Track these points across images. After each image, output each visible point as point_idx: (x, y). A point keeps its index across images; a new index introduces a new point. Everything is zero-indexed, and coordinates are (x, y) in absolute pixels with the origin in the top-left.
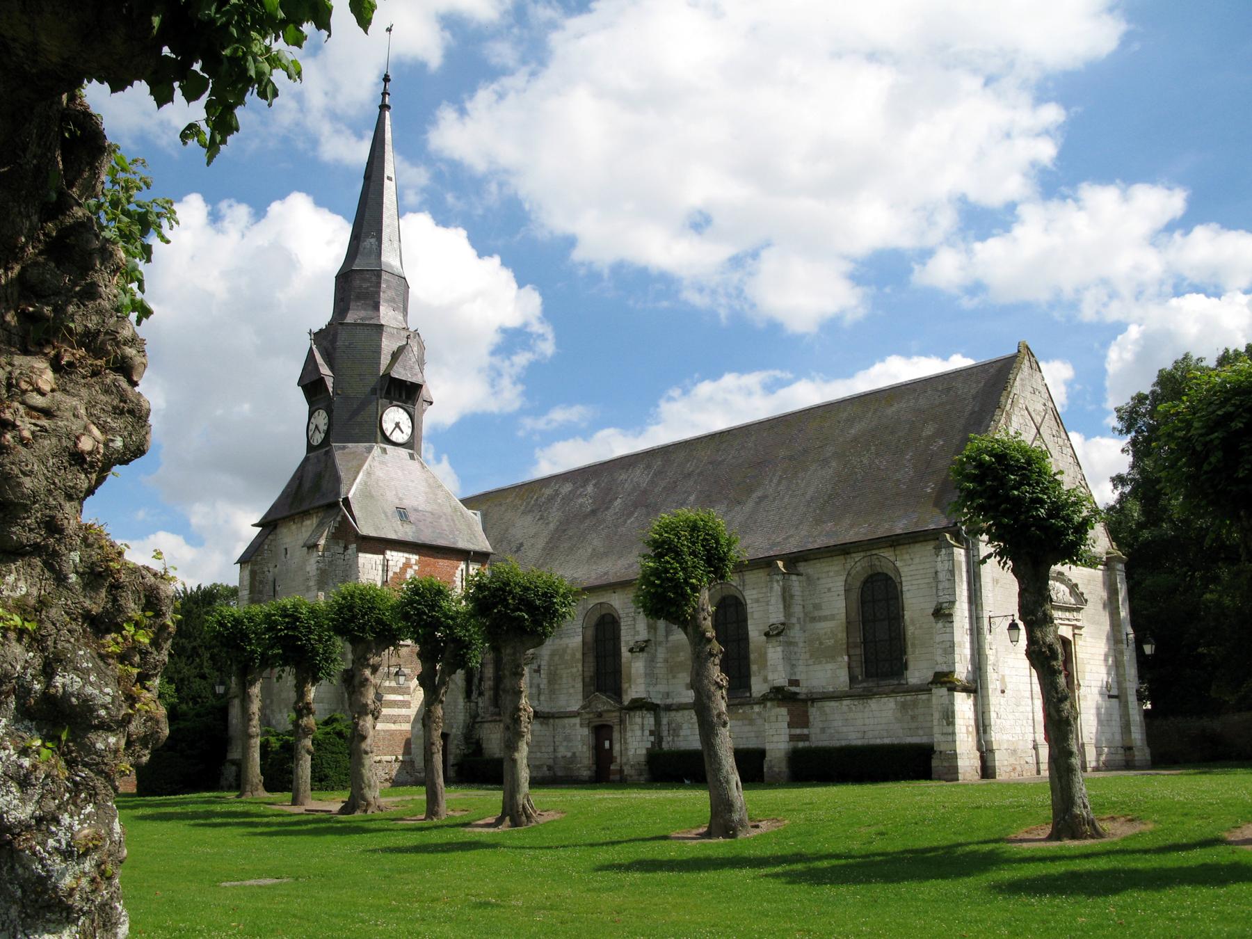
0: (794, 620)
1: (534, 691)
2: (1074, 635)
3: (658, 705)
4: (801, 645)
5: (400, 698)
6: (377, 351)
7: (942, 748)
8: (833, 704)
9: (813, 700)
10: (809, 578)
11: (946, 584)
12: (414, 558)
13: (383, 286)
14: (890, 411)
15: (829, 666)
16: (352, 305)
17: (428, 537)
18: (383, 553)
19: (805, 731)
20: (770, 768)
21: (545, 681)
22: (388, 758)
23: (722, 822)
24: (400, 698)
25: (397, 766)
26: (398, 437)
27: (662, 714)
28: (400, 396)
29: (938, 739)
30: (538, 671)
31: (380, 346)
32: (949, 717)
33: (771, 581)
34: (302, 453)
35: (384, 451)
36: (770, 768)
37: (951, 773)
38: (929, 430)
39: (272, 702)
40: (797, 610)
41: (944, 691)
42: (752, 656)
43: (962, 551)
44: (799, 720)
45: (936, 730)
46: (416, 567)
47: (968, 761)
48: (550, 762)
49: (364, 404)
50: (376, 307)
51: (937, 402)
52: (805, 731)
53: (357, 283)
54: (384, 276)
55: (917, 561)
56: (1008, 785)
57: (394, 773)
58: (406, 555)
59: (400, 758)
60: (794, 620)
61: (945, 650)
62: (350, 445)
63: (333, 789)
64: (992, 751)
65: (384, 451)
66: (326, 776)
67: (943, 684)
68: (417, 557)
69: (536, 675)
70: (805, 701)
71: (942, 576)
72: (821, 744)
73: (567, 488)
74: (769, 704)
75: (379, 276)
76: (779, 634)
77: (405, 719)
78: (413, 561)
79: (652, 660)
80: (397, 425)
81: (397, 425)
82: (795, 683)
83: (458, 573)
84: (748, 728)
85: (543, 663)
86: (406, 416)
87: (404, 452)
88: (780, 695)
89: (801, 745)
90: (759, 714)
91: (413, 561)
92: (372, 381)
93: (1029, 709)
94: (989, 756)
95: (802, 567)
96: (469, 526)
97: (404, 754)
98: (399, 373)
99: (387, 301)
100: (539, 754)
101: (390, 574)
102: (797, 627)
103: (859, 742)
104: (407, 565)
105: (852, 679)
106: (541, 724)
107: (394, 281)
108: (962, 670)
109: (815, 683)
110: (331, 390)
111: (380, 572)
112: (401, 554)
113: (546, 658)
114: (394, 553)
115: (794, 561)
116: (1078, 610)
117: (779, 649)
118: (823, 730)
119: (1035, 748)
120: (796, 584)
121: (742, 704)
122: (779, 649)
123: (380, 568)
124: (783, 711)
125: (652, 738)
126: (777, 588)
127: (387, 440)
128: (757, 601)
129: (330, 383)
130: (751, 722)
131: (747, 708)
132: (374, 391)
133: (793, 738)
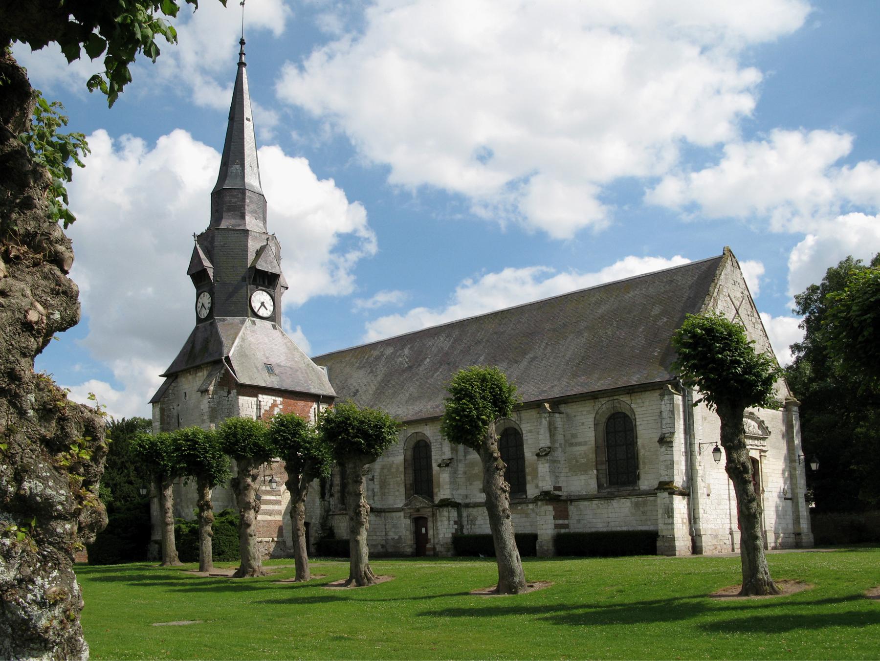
0: (557, 445)
1: (370, 493)
2: (761, 456)
3: (459, 504)
4: (562, 462)
5: (274, 498)
6: (245, 250)
8: (586, 503)
9: (572, 501)
10: (568, 415)
11: (668, 421)
12: (279, 400)
13: (247, 201)
14: (628, 296)
15: (583, 477)
16: (225, 215)
17: (288, 385)
18: (256, 396)
19: (566, 522)
20: (541, 547)
21: (378, 487)
22: (267, 539)
24: (274, 498)
25: (273, 545)
26: (263, 312)
27: (463, 510)
28: (264, 282)
29: (661, 528)
30: (372, 479)
31: (247, 246)
32: (669, 512)
33: (541, 417)
34: (194, 324)
35: (254, 323)
36: (541, 547)
37: (671, 550)
38: (656, 311)
39: (181, 500)
40: (560, 438)
41: (666, 494)
42: (527, 470)
43: (680, 397)
45: (660, 521)
46: (281, 407)
48: (383, 542)
49: (237, 289)
50: (243, 217)
52: (566, 522)
53: (227, 199)
54: (248, 194)
55: (647, 403)
56: (711, 559)
57: (271, 550)
58: (273, 398)
59: (276, 539)
60: (557, 445)
61: (667, 466)
62: (228, 318)
63: (228, 560)
64: (700, 536)
65: (254, 323)
66: (223, 552)
67: (665, 490)
68: (281, 399)
69: (370, 482)
70: (566, 501)
72: (577, 530)
73: (390, 350)
74: (540, 503)
75: (244, 194)
76: (546, 455)
77: (278, 512)
78: (279, 402)
79: (455, 472)
80: (263, 304)
81: (263, 304)
83: (312, 411)
85: (376, 474)
86: (268, 297)
87: (268, 324)
88: (548, 497)
89: (563, 531)
91: (279, 402)
92: (242, 272)
93: (727, 507)
94: (698, 539)
95: (563, 408)
96: (319, 378)
97: (278, 537)
98: (261, 266)
99: (251, 212)
100: (375, 537)
101: (262, 411)
102: (560, 450)
103: (605, 530)
104: (274, 405)
105: (600, 486)
106: (376, 516)
107: (255, 197)
108: (679, 480)
110: (212, 278)
111: (255, 410)
112: (269, 397)
113: (378, 470)
114: (265, 396)
115: (557, 403)
116: (764, 439)
117: (547, 465)
118: (579, 521)
119: (731, 533)
120: (559, 419)
121: (520, 503)
122: (547, 465)
123: (255, 407)
125: (456, 526)
126: (545, 422)
127: (256, 315)
128: (530, 431)
129: (211, 273)
130: (527, 515)
131: (524, 506)
132: (244, 279)
133: (557, 526)
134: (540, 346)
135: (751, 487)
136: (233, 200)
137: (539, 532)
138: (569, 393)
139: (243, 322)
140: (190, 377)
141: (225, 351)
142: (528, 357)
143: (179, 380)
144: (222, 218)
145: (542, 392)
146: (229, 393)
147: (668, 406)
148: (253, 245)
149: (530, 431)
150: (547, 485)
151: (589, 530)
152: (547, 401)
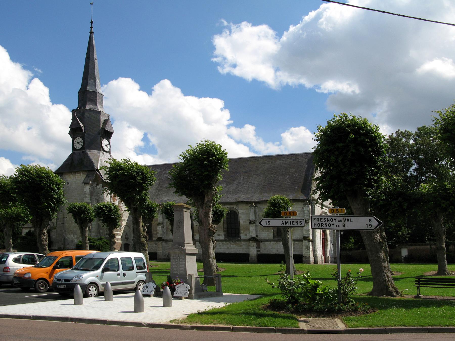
7: (306, 255)
8: (268, 243)
9: (262, 241)
10: (260, 208)
11: (307, 214)
14: (279, 162)
15: (267, 233)
16: (87, 103)
20: (251, 259)
23: (442, 271)
29: (304, 253)
30: (163, 227)
31: (100, 119)
32: (308, 248)
33: (251, 208)
34: (70, 152)
35: (103, 154)
36: (251, 259)
37: (309, 262)
38: (292, 170)
39: (65, 231)
40: (257, 216)
41: (307, 241)
42: (241, 228)
44: (258, 247)
45: (304, 251)
47: (312, 259)
50: (96, 105)
51: (293, 162)
54: (98, 94)
55: (296, 207)
61: (307, 231)
64: (317, 257)
65: (103, 154)
67: (306, 239)
71: (306, 212)
72: (264, 253)
73: (158, 170)
74: (251, 242)
75: (97, 94)
76: (254, 223)
82: (257, 236)
84: (239, 248)
88: (254, 239)
89: (259, 253)
90: (243, 244)
94: (316, 258)
95: (258, 205)
103: (277, 253)
105: (274, 236)
107: (101, 96)
108: (311, 237)
109: (262, 237)
115: (256, 203)
117: (254, 227)
118: (265, 249)
119: (321, 257)
121: (238, 241)
122: (254, 227)
124: (255, 244)
126: (252, 210)
128: (243, 213)
129: (83, 129)
130: (241, 246)
131: (239, 242)
132: (99, 133)
133: (258, 251)
134: (240, 178)
135: (410, 244)
136: (92, 96)
137: (250, 253)
138: (262, 200)
139: (99, 153)
140: (71, 175)
141: (95, 165)
142: (235, 182)
143: (63, 176)
144: (86, 104)
145: (248, 198)
146: (97, 185)
147: (307, 209)
148: (102, 119)
149: (243, 213)
150: (254, 235)
151: (272, 253)
152: (253, 202)
